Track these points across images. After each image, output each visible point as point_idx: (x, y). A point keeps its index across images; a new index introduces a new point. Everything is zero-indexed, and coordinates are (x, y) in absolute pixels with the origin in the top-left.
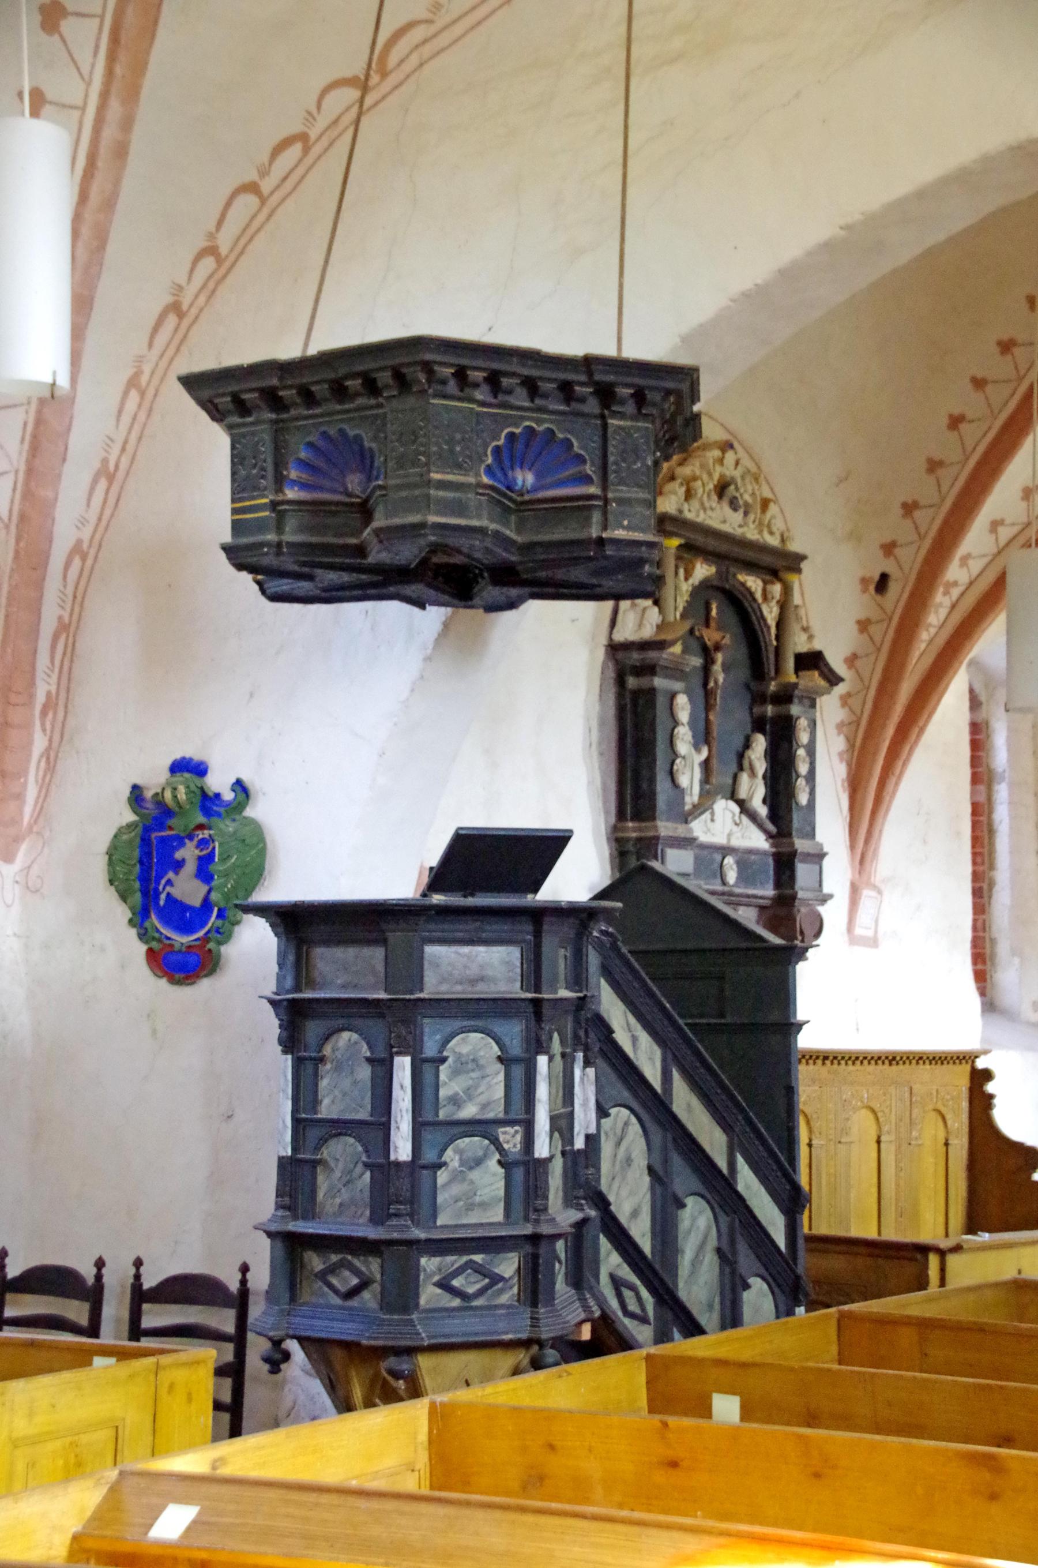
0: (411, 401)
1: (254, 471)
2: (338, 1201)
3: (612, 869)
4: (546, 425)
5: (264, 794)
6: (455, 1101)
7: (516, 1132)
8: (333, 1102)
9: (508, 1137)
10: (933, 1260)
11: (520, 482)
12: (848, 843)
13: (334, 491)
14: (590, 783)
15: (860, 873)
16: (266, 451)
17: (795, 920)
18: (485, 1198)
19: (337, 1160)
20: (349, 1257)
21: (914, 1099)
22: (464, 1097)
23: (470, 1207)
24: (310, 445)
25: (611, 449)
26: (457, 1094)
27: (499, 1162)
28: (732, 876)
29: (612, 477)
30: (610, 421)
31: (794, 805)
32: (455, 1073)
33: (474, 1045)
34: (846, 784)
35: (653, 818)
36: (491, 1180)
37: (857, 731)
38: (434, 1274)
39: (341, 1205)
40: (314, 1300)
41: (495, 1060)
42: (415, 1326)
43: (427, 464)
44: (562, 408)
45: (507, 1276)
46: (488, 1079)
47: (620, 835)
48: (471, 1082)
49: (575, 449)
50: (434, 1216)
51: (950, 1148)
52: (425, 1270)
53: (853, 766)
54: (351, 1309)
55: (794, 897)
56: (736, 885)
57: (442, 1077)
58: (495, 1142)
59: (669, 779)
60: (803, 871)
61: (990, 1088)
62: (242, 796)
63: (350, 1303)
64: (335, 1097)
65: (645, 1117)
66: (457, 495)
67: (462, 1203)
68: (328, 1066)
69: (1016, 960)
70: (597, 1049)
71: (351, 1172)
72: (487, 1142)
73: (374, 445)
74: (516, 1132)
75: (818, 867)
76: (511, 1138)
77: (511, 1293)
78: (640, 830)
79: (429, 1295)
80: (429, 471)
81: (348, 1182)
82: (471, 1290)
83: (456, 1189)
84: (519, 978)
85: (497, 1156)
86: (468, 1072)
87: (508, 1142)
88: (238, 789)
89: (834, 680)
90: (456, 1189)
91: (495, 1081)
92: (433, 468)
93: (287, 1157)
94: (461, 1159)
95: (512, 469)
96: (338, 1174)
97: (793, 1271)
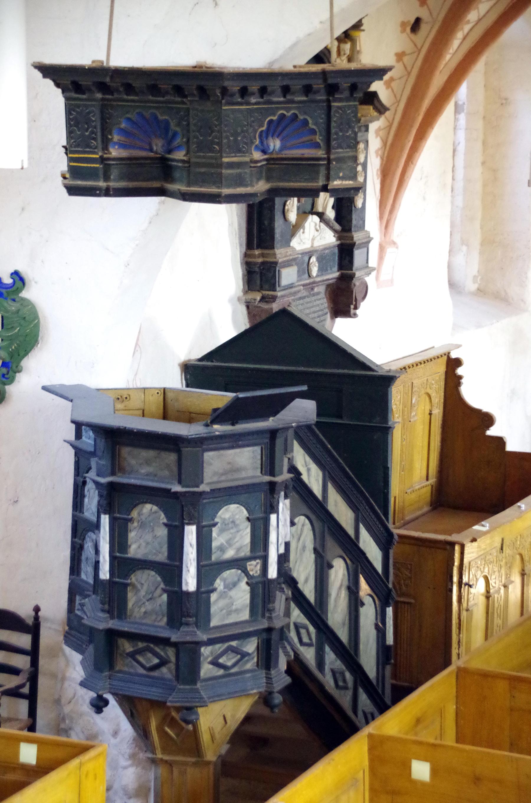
0: (208, 106)
1: (87, 134)
2: (143, 610)
3: (244, 285)
4: (292, 112)
5: (36, 282)
6: (222, 549)
7: (257, 563)
8: (139, 547)
9: (252, 567)
10: (457, 548)
11: (272, 148)
12: (378, 215)
13: (141, 148)
14: (231, 225)
15: (385, 236)
16: (96, 118)
17: (352, 291)
18: (239, 607)
19: (142, 584)
20: (152, 646)
21: (414, 390)
22: (227, 546)
23: (229, 613)
24: (129, 119)
25: (333, 124)
26: (222, 544)
27: (247, 583)
28: (315, 271)
29: (333, 143)
30: (333, 104)
31: (353, 208)
32: (222, 531)
33: (234, 513)
34: (379, 173)
35: (273, 248)
36: (242, 595)
37: (389, 133)
38: (208, 657)
39: (145, 613)
40: (126, 669)
41: (245, 520)
42: (200, 693)
43: (220, 151)
44: (305, 98)
45: (250, 651)
46: (241, 532)
47: (250, 260)
48: (231, 535)
49: (310, 125)
50: (209, 621)
51: (432, 416)
52: (203, 655)
53: (385, 159)
54: (153, 678)
55: (352, 277)
56: (317, 276)
57: (214, 534)
58: (245, 572)
59: (282, 216)
60: (358, 255)
61: (460, 371)
62: (19, 284)
63: (152, 674)
64: (140, 545)
65: (313, 517)
66: (239, 171)
67: (225, 611)
68: (135, 524)
69: (464, 248)
70: (292, 486)
71: (153, 593)
72: (240, 571)
73: (178, 129)
74: (257, 563)
75: (366, 249)
76: (254, 567)
77: (253, 661)
78: (263, 255)
79: (206, 670)
80: (222, 157)
81: (151, 599)
82: (229, 664)
83: (222, 603)
84: (260, 466)
85: (246, 579)
86: (229, 529)
87: (252, 570)
88: (17, 278)
89: (382, 110)
90: (222, 603)
91: (245, 532)
92: (224, 155)
93: (107, 580)
94: (224, 584)
95: (267, 138)
96: (142, 593)
97: (387, 587)
